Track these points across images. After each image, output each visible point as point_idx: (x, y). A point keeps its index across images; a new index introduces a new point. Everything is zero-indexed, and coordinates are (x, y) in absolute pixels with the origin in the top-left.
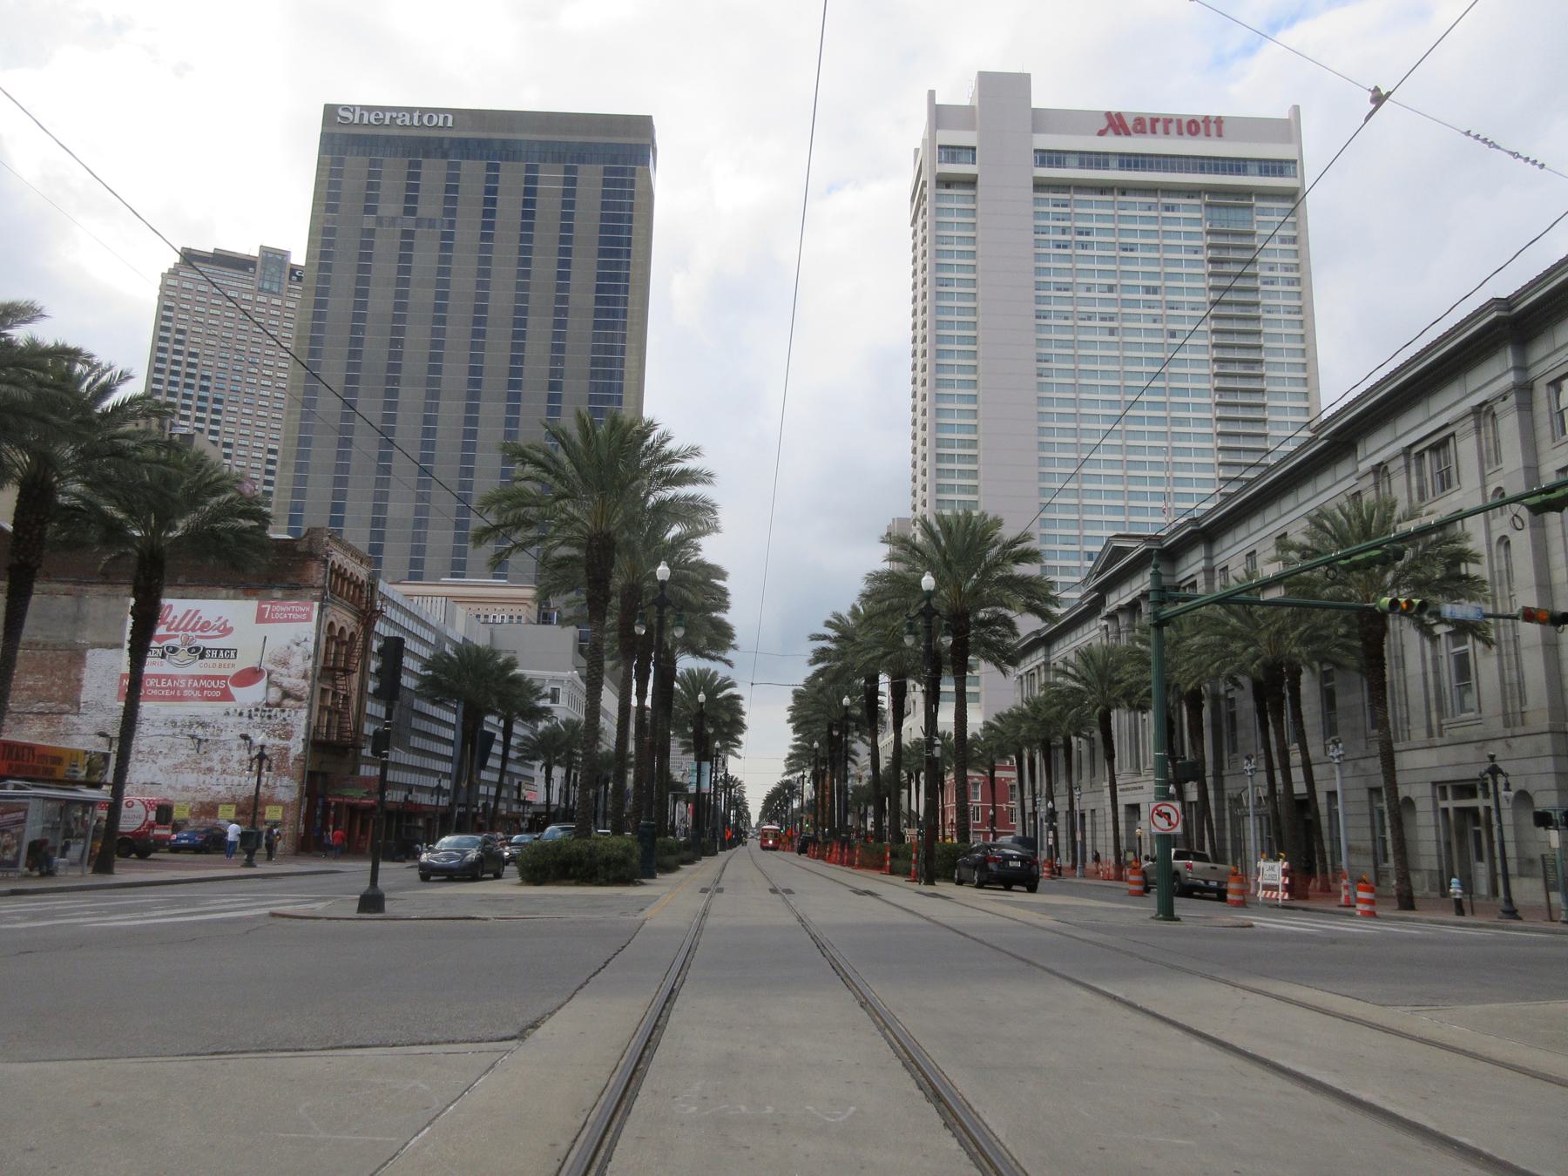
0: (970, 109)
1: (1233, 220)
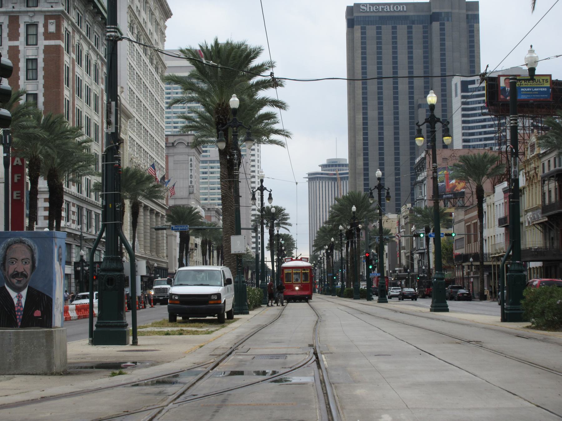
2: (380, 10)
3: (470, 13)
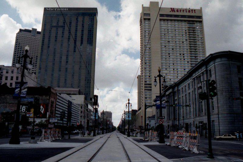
0: (149, 7)
1: (192, 26)
2: (55, 10)
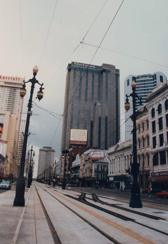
2: (83, 66)
3: (117, 73)
